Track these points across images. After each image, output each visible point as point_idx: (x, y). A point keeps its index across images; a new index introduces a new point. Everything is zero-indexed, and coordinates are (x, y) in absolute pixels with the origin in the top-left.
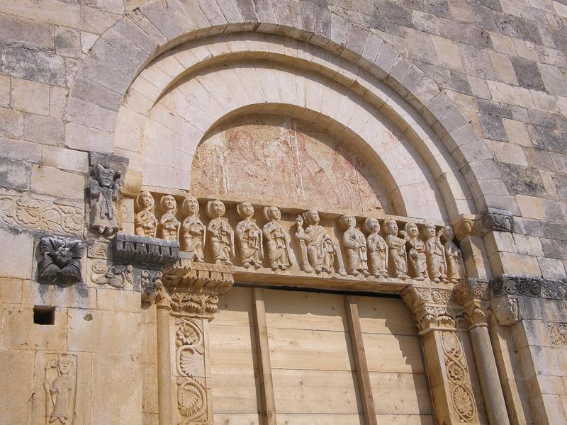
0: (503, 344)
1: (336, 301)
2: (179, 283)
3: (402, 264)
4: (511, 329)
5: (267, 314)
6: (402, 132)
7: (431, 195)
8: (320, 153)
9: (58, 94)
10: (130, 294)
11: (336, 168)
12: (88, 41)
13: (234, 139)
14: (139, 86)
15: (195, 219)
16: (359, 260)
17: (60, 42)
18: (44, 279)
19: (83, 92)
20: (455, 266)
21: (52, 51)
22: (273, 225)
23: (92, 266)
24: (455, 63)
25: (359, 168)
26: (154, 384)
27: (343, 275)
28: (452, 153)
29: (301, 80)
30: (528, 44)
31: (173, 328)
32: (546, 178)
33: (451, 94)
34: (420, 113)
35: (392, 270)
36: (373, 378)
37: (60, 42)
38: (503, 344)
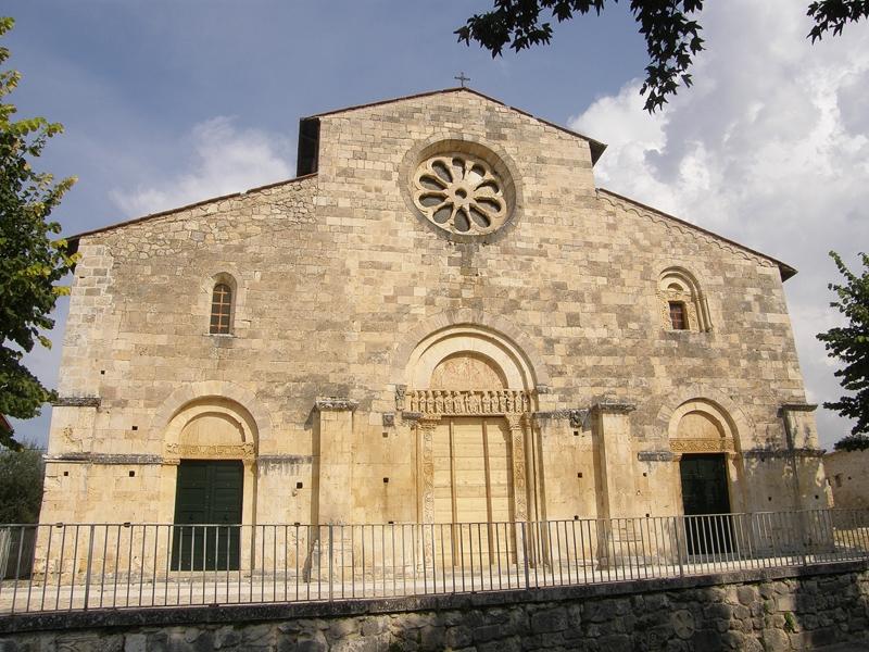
0: (535, 434)
1: (481, 420)
2: (421, 421)
3: (503, 407)
8: (480, 365)
9: (387, 368)
10: (408, 428)
12: (396, 345)
14: (412, 356)
15: (431, 398)
16: (487, 407)
17: (388, 348)
18: (385, 425)
19: (395, 365)
20: (525, 406)
23: (397, 421)
26: (357, 124)
27: (481, 413)
28: (529, 363)
29: (472, 339)
30: (578, 304)
31: (422, 434)
32: (569, 368)
38: (535, 434)
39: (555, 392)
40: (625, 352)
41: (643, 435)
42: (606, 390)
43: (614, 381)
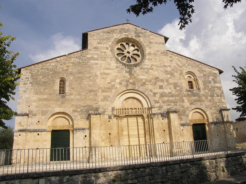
0: (151, 120)
2: (119, 117)
3: (142, 112)
4: (152, 118)
6: (144, 98)
7: (147, 104)
8: (135, 101)
13: (126, 101)
16: (138, 112)
17: (109, 97)
18: (109, 118)
19: (111, 101)
20: (148, 112)
21: (108, 98)
22: (129, 110)
23: (112, 117)
24: (151, 88)
25: (96, 178)
31: (120, 120)
32: (160, 101)
34: (146, 96)
35: (141, 113)
36: (139, 123)
37: (109, 97)
38: (151, 120)
39: (156, 108)
40: (176, 96)
41: (182, 119)
42: (171, 106)
43: (173, 104)
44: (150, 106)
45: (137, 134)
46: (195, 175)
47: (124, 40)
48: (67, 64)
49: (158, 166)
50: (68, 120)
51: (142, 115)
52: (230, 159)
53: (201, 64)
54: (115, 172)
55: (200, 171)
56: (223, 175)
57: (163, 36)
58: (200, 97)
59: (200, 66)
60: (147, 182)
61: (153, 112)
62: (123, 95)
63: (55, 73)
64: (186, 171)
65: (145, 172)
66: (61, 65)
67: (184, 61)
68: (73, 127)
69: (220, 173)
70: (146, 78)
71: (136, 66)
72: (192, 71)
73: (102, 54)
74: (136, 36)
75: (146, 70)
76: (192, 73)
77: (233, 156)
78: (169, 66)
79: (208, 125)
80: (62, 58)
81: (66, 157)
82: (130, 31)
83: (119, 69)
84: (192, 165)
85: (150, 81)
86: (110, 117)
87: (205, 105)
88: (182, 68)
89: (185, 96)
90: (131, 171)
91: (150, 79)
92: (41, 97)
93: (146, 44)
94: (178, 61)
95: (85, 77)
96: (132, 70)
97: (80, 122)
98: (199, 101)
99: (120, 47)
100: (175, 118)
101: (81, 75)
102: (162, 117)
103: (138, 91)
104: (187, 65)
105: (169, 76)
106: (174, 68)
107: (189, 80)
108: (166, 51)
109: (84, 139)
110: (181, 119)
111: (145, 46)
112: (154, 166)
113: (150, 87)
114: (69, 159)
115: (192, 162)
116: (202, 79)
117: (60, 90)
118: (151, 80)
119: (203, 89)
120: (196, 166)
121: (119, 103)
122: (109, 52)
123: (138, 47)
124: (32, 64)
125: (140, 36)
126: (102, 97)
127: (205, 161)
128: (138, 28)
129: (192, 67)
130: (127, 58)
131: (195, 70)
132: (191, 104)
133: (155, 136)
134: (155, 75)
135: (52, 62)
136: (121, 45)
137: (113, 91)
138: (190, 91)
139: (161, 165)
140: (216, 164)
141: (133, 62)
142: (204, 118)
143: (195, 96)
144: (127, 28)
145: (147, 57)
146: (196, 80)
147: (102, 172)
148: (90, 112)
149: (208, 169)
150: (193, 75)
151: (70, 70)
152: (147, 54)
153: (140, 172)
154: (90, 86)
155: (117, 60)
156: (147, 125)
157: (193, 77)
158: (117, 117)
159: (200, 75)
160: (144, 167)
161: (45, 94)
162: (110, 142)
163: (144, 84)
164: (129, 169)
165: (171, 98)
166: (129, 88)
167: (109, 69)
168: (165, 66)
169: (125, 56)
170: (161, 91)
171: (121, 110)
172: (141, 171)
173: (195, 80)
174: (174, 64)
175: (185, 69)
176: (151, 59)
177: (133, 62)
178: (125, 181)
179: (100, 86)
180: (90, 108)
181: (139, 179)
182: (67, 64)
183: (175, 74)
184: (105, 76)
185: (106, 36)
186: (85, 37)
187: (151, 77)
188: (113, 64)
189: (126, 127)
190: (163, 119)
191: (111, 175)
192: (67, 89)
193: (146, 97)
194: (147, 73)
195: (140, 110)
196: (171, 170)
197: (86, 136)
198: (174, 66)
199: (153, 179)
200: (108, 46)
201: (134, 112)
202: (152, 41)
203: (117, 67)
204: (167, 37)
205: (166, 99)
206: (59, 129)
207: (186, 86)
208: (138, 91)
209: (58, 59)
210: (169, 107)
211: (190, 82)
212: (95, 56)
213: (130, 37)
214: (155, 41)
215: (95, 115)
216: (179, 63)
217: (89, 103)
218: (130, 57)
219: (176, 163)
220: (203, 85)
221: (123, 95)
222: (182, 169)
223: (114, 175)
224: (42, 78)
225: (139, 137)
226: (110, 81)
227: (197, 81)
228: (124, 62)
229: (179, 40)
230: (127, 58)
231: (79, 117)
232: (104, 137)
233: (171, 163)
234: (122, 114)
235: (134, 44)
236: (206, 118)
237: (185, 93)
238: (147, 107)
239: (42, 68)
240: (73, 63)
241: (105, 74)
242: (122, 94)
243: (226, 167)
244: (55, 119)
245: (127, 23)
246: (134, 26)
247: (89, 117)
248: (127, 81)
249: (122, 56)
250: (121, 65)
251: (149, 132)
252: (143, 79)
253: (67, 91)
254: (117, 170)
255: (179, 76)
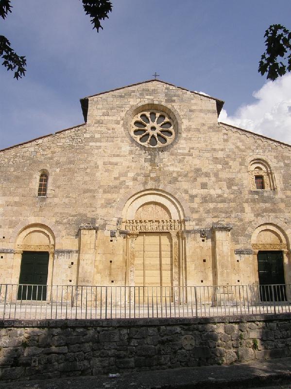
0: (183, 241)
2: (129, 235)
3: (169, 228)
5: (18, 260)
6: (174, 203)
8: (159, 208)
11: (161, 210)
17: (114, 201)
18: (111, 236)
23: (117, 234)
24: (186, 187)
33: (183, 195)
40: (230, 201)
42: (219, 219)
43: (224, 215)
44: (182, 218)
45: (159, 263)
46: (189, 350)
47: (147, 108)
48: (52, 149)
49: (113, 327)
50: (48, 236)
51: (169, 232)
52: (273, 325)
53: (282, 145)
54: (29, 330)
55: (201, 344)
56: (252, 355)
57: (214, 99)
58: (275, 204)
59: (279, 148)
60: (87, 354)
61: (187, 228)
62: (139, 197)
63: (33, 162)
64: (171, 341)
65: (86, 334)
66: (44, 150)
67: (249, 140)
68: (54, 245)
69: (247, 351)
70: (179, 169)
71: (162, 150)
72: (264, 158)
73: (109, 131)
74: (167, 101)
75: (179, 157)
76: (263, 161)
77: (280, 320)
78: (222, 150)
79: (288, 254)
80: (46, 139)
81: (41, 295)
82: (158, 94)
83: (133, 156)
84: (186, 330)
85: (186, 176)
86: (113, 235)
87: (285, 219)
88: (244, 153)
89: (247, 201)
90: (58, 330)
91: (186, 172)
92: (12, 199)
93: (183, 113)
94: (238, 140)
95: (78, 169)
96: (155, 156)
97: (66, 242)
98: (273, 211)
99: (139, 119)
100: (224, 240)
101: (72, 165)
102: (201, 237)
103: (163, 191)
104: (254, 147)
105: (220, 167)
106: (231, 153)
107: (257, 174)
108: (219, 123)
109: (69, 267)
110: (237, 242)
111: (181, 116)
112: (104, 325)
113: (185, 185)
114: (44, 299)
115: (186, 325)
116: (282, 171)
117: (40, 190)
118: (187, 174)
119: (282, 190)
120: (195, 334)
121: (130, 211)
122: (120, 129)
123: (170, 118)
124: (9, 147)
125: (174, 101)
126: (103, 202)
127: (215, 326)
128: (171, 87)
129: (264, 152)
130: (150, 137)
131: (269, 157)
132: (257, 215)
133: (188, 269)
134: (195, 165)
135: (31, 146)
136: (142, 116)
137: (122, 191)
138: (256, 193)
139: (118, 325)
140: (240, 332)
141: (159, 144)
142: (281, 241)
143: (265, 202)
144: (153, 88)
145: (184, 135)
146: (270, 174)
147: (6, 327)
148: (82, 225)
149: (220, 341)
150: (264, 166)
151: (55, 159)
152: (183, 130)
153: (75, 334)
154: (85, 183)
155: (133, 140)
156: (175, 250)
157: (264, 169)
158: (125, 234)
159: (278, 165)
160: (84, 325)
161: (17, 196)
162: (110, 275)
163: (175, 180)
164: (56, 327)
165: (220, 205)
166: (148, 187)
167: (118, 156)
168: (215, 150)
169: (148, 135)
170: (203, 192)
171: (133, 223)
172: (78, 332)
173: (268, 175)
174: (230, 146)
175: (251, 154)
176: (190, 139)
177: (159, 144)
178: (44, 347)
179: (102, 184)
180: (83, 218)
181: (72, 346)
182: (52, 149)
183: (230, 164)
184: (110, 167)
185: (118, 103)
186: (85, 104)
187: (188, 168)
188: (126, 147)
189: (141, 252)
190: (203, 241)
191: (21, 335)
192: (50, 187)
193: (177, 202)
194: (180, 161)
195: (165, 224)
196: (139, 336)
197: (72, 263)
198: (231, 150)
199: (99, 349)
200: (119, 119)
201: (153, 227)
202: (193, 108)
203: (131, 152)
204: (220, 99)
205: (211, 206)
206: (33, 250)
207: (249, 183)
208: (163, 191)
209: (40, 141)
210: (215, 220)
211: (258, 177)
212: (97, 136)
213: (156, 102)
214: (200, 108)
215: (88, 229)
216: (239, 144)
217: (81, 210)
218: (160, 133)
219: (150, 324)
220: (282, 183)
221: (139, 197)
222: (162, 337)
223: (26, 335)
224: (14, 171)
225: (161, 270)
226: (118, 176)
227: (272, 175)
228: (145, 144)
229: (288, 109)
230: (150, 137)
231: (64, 233)
232: (101, 267)
233: (141, 323)
234: (135, 229)
235: (164, 114)
236: (284, 241)
237: (247, 196)
238: (178, 219)
239: (16, 156)
240: (62, 147)
241: (111, 163)
242: (139, 195)
243: (262, 340)
244: (29, 234)
245: (154, 81)
246: (165, 85)
247: (78, 235)
248: (147, 176)
249: (143, 134)
250: (139, 149)
251: (179, 262)
252: (174, 171)
253: (48, 192)
254: (33, 327)
255: (239, 167)
